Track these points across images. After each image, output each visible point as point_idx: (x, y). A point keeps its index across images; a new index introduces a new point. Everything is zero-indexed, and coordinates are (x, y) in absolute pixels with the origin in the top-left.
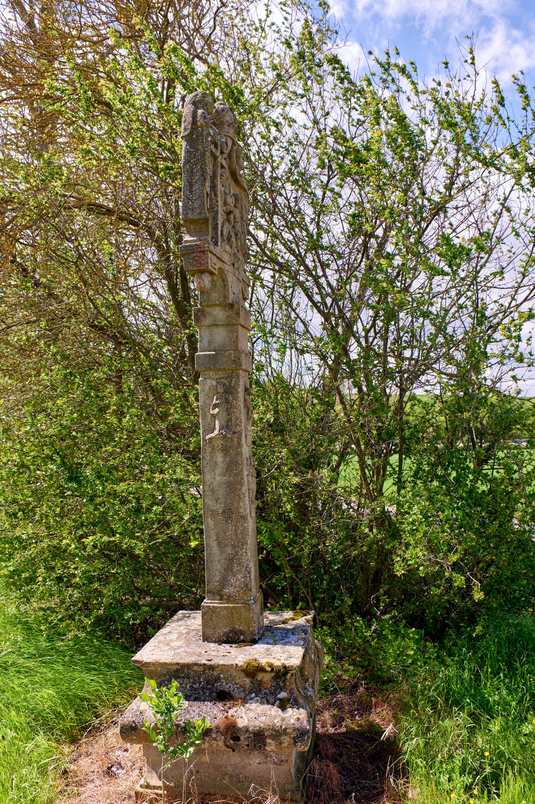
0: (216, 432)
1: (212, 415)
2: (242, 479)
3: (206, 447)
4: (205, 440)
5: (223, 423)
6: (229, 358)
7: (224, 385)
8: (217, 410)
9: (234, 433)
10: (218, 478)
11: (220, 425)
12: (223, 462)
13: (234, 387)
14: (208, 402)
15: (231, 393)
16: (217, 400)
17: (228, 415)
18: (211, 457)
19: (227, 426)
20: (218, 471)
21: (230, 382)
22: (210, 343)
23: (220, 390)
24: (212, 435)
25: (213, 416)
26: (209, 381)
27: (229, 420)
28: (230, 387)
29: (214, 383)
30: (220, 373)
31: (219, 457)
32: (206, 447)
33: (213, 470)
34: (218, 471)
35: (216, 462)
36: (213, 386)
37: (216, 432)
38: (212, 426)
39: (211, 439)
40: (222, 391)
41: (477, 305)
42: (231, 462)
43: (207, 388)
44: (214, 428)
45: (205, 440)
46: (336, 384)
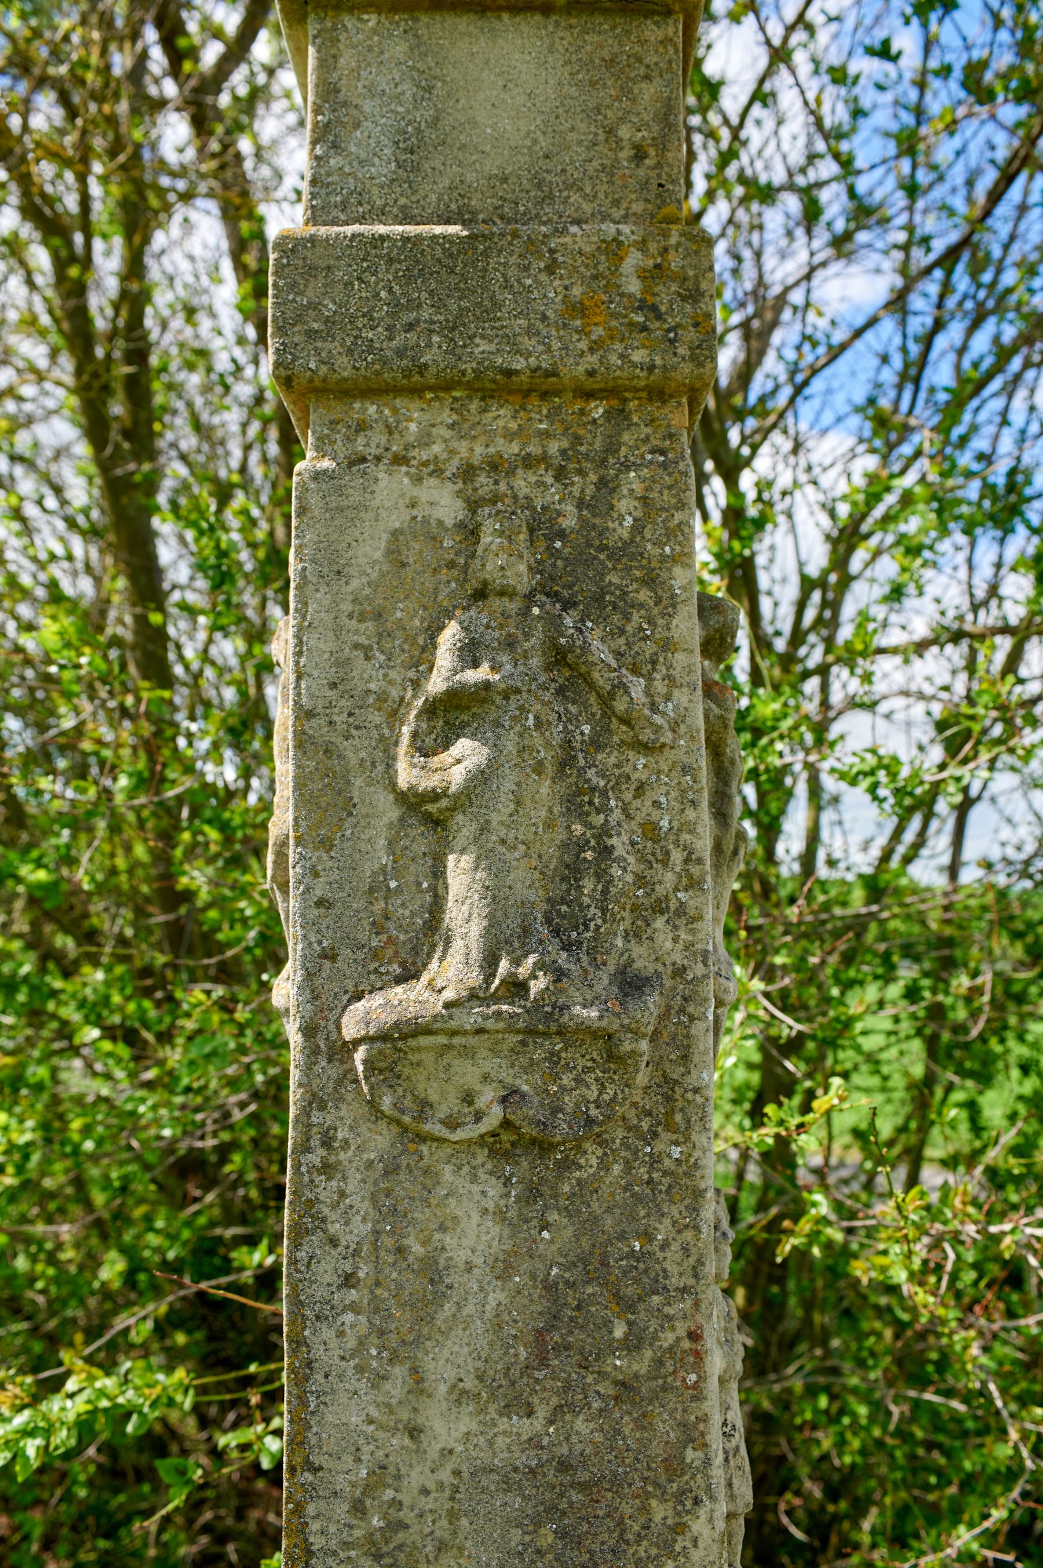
0: (451, 972)
1: (413, 803)
2: (692, 1434)
3: (344, 1118)
4: (326, 1045)
5: (526, 884)
6: (606, 280)
7: (542, 526)
8: (464, 757)
9: (631, 984)
10: (448, 1428)
11: (495, 897)
12: (503, 1268)
13: (625, 553)
14: (369, 676)
15: (602, 605)
16: (470, 653)
17: (578, 802)
18: (390, 1212)
19: (563, 912)
20: (450, 1360)
21: (598, 503)
22: (412, 151)
23: (505, 561)
24: (411, 1000)
25: (429, 815)
26: (390, 487)
27: (580, 862)
28: (593, 547)
29: (445, 504)
30: (502, 416)
31: (471, 1218)
32: (344, 1118)
33: (400, 1344)
34: (450, 1360)
35: (433, 1271)
36: (428, 531)
37: (451, 972)
38: (408, 910)
39: (396, 1039)
40: (520, 575)
41: (168, 42)
42: (591, 1264)
43: (369, 551)
44: (431, 932)
45: (326, 1045)
46: (869, 1165)
